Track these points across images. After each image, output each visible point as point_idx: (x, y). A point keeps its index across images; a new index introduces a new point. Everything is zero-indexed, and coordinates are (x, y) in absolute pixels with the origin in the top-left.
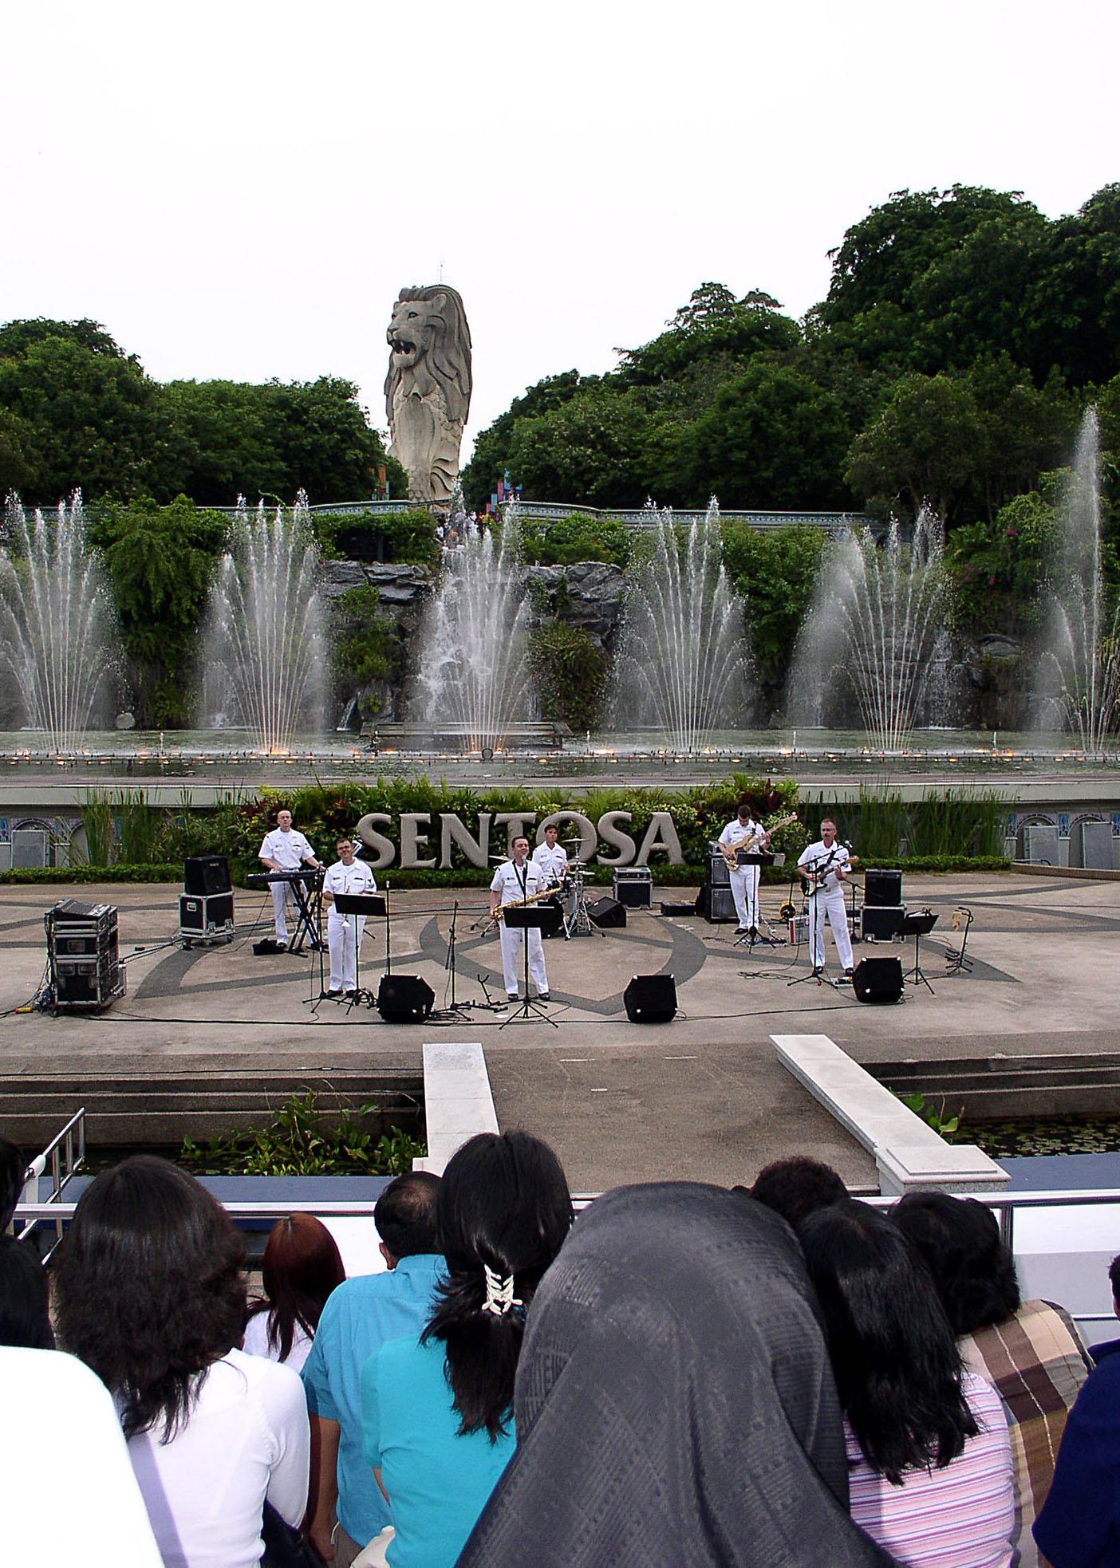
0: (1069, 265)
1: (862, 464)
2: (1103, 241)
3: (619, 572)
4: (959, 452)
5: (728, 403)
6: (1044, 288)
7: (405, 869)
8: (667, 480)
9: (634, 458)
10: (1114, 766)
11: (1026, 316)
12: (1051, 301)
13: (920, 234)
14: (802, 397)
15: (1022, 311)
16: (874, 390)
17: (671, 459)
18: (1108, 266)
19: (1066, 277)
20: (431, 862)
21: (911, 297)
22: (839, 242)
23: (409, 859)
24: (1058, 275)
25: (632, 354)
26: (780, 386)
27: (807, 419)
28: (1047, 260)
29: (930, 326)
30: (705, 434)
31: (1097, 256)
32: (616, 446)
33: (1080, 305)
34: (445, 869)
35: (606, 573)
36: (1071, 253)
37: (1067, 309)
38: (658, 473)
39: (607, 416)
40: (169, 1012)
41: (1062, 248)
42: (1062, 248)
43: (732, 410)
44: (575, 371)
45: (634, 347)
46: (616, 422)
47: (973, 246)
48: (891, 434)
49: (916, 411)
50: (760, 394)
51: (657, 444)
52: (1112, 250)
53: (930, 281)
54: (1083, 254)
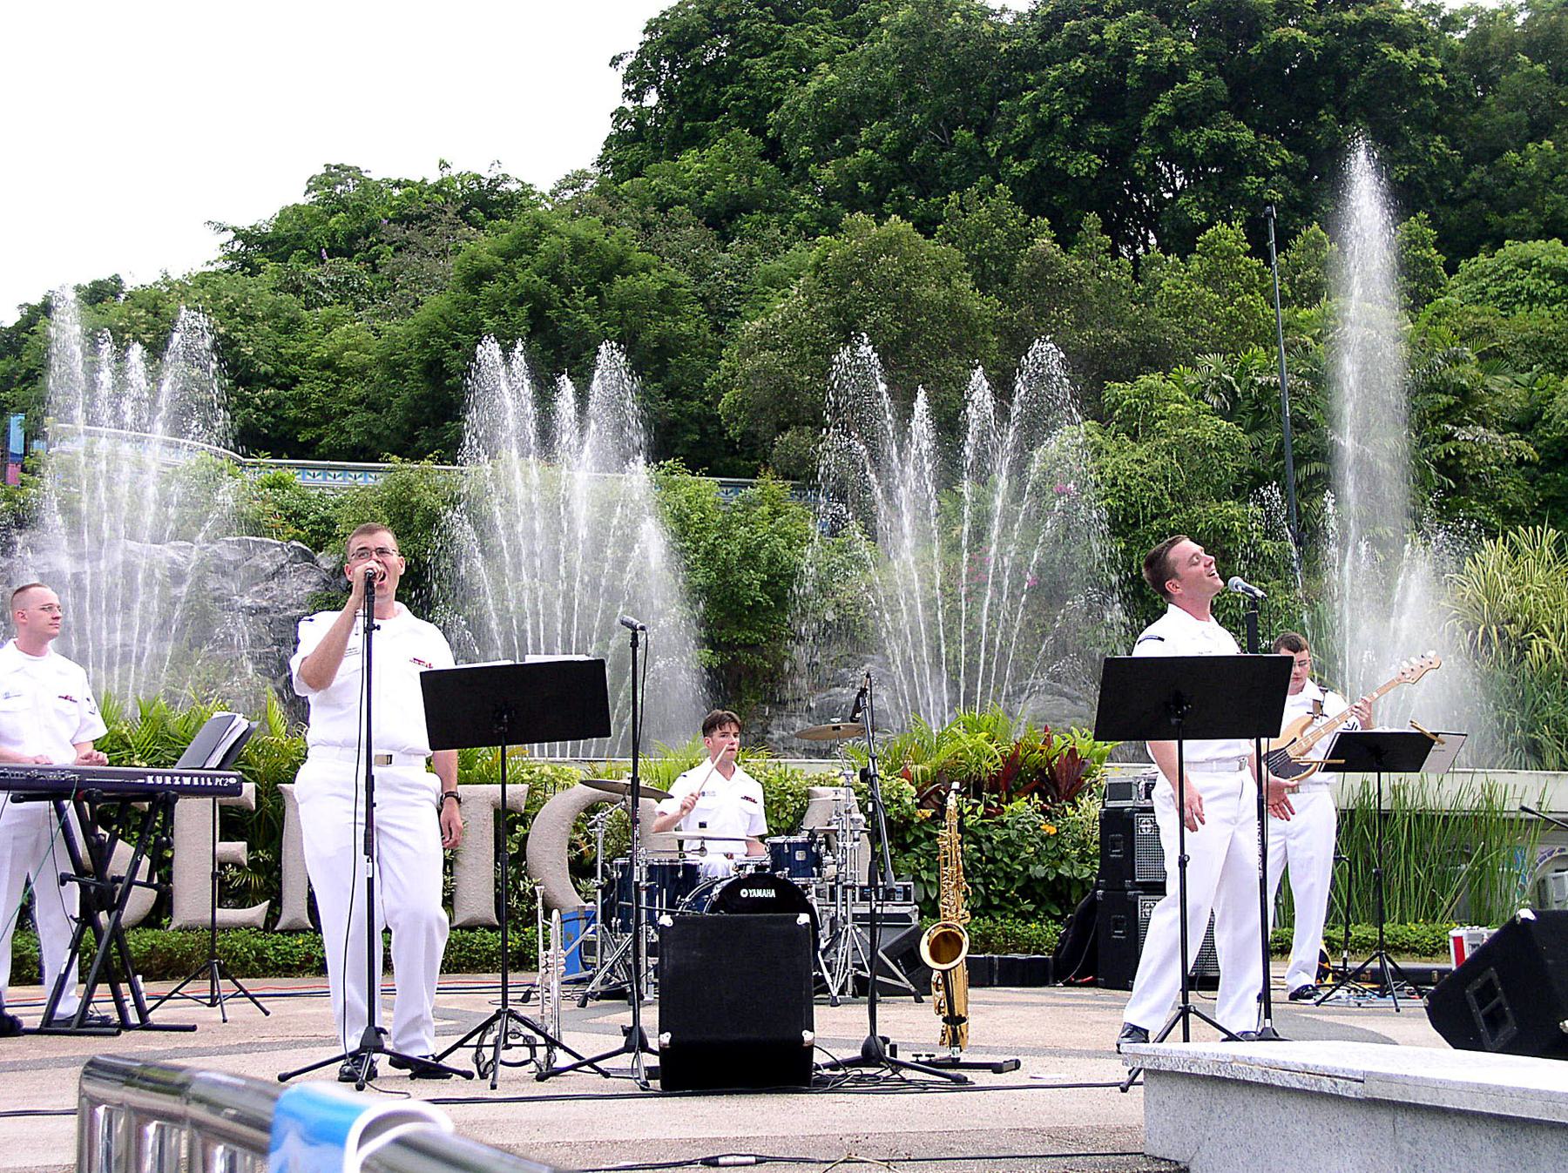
0: (1077, 65)
1: (766, 372)
2: (1137, 25)
3: (308, 557)
4: (944, 354)
5: (476, 278)
6: (1035, 106)
7: (180, 929)
8: (355, 425)
9: (287, 388)
10: (178, 1168)
11: (999, 156)
12: (1046, 128)
13: (781, 32)
14: (620, 266)
15: (992, 148)
16: (739, 273)
17: (357, 390)
18: (1147, 68)
19: (1076, 86)
20: (257, 913)
21: (781, 126)
22: (632, 40)
23: (194, 899)
24: (1059, 82)
25: (240, 235)
26: (579, 249)
27: (633, 306)
28: (1030, 61)
29: (828, 173)
30: (435, 332)
31: (1128, 51)
32: (249, 363)
33: (1098, 135)
34: (291, 931)
35: (282, 559)
36: (1076, 45)
37: (1075, 142)
38: (328, 419)
39: (229, 308)
40: (485, 1151)
41: (1057, 41)
42: (1057, 41)
43: (489, 288)
44: (117, 280)
45: (245, 223)
46: (249, 319)
47: (900, 32)
48: (816, 315)
49: (860, 275)
50: (540, 261)
51: (327, 364)
52: (1151, 40)
53: (821, 94)
54: (1099, 50)
